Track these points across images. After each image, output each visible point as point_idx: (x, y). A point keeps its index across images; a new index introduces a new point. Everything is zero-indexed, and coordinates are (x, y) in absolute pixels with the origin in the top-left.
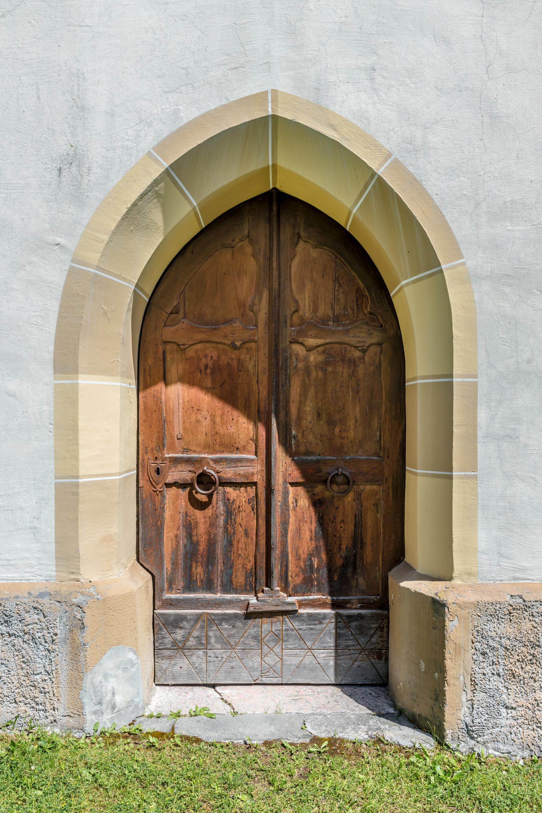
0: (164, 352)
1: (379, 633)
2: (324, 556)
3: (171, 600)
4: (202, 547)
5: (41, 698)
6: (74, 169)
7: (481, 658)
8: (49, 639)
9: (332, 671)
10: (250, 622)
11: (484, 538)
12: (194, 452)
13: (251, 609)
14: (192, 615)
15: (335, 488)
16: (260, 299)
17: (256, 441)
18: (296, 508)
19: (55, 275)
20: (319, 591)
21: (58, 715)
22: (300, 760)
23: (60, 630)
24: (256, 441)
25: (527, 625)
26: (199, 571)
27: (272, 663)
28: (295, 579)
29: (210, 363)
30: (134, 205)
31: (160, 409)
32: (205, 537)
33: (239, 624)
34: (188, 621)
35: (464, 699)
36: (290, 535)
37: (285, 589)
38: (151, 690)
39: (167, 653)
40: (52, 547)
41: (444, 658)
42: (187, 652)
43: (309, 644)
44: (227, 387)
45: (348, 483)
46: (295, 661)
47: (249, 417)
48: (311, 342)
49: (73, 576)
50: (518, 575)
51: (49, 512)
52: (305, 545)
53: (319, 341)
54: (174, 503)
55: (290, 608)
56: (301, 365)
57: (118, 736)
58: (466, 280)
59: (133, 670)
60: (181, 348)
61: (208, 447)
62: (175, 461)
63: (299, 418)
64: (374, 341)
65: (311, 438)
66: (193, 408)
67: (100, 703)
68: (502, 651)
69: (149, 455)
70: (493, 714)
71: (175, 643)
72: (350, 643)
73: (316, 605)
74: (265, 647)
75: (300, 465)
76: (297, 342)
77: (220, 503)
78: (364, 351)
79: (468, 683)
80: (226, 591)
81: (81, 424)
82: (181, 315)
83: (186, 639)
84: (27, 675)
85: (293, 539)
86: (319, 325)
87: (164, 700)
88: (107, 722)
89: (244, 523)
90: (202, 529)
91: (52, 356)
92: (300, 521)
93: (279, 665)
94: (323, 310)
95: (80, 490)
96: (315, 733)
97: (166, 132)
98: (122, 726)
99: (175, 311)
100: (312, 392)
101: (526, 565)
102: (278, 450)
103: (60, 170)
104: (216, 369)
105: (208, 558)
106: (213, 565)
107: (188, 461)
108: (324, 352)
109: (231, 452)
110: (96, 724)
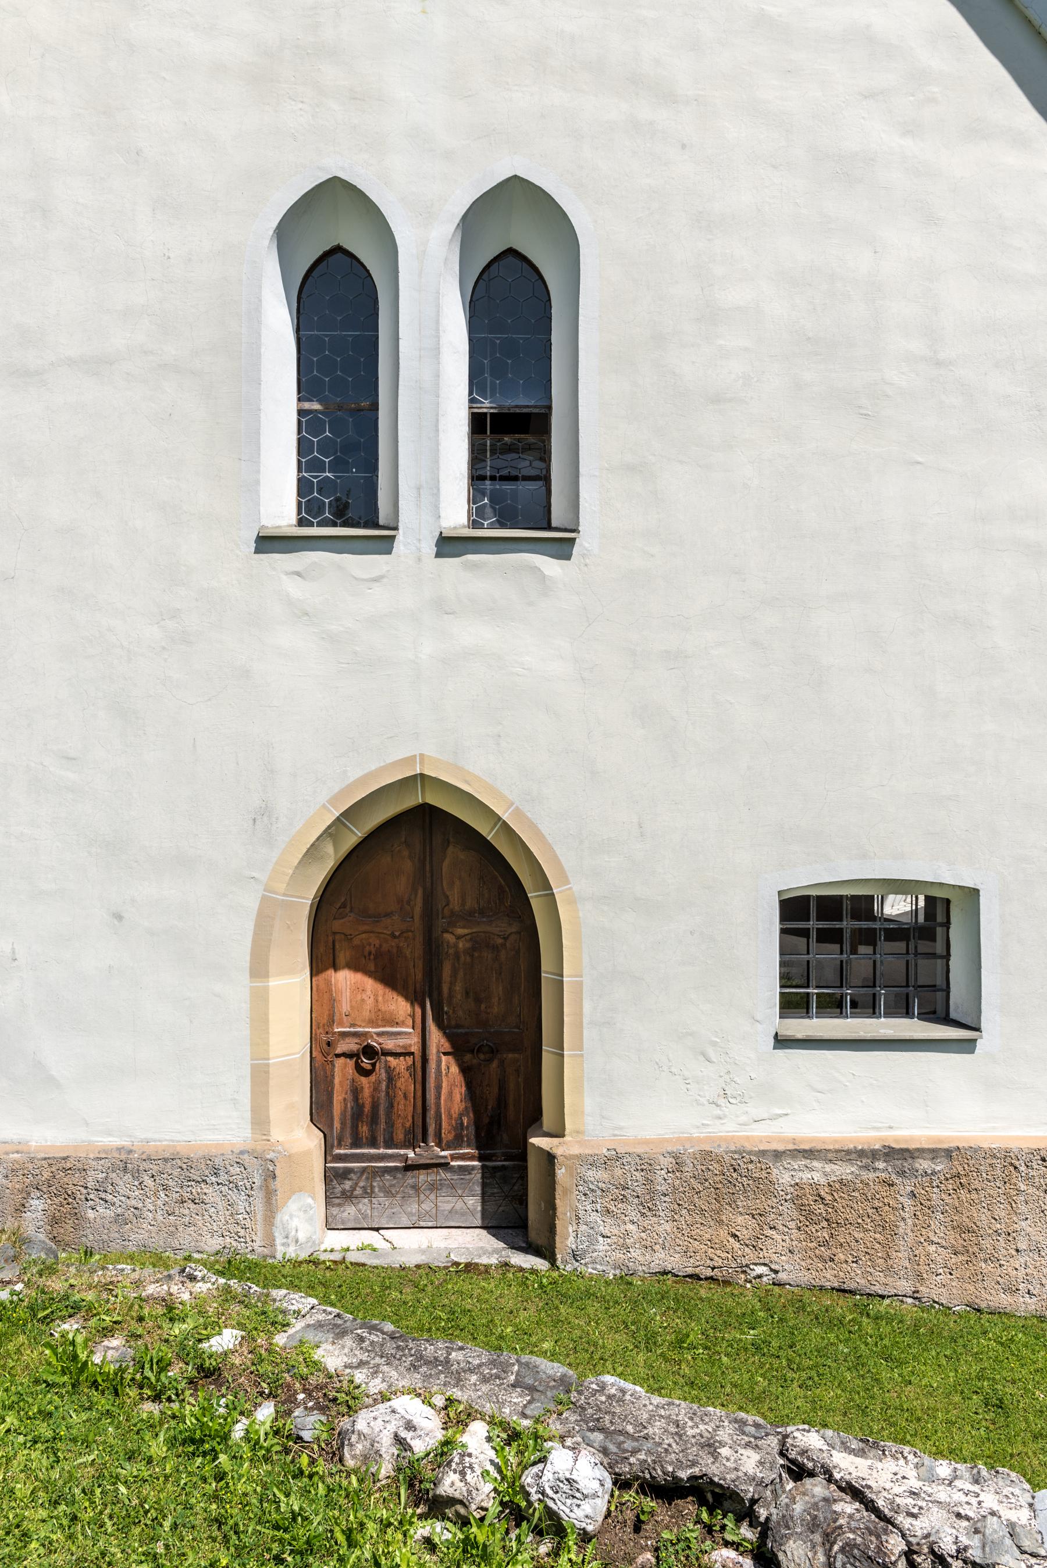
0: (334, 942)
1: (520, 1182)
2: (471, 1115)
3: (340, 1155)
4: (367, 1109)
5: (242, 1233)
6: (265, 818)
7: (583, 1198)
8: (249, 1187)
9: (479, 1215)
10: (409, 1173)
11: (589, 1103)
12: (360, 1026)
13: (410, 1162)
14: (358, 1167)
15: (482, 1056)
16: (416, 895)
17: (413, 1016)
18: (448, 1076)
19: (251, 901)
20: (469, 1146)
21: (256, 1245)
22: (440, 1276)
23: (258, 1180)
24: (413, 1016)
25: (618, 1172)
26: (364, 1130)
27: (428, 1209)
28: (447, 1135)
29: (373, 951)
30: (312, 845)
31: (331, 991)
32: (369, 1100)
33: (399, 1176)
34: (355, 1173)
35: (571, 1231)
36: (443, 1098)
37: (439, 1144)
38: (324, 1232)
39: (337, 1201)
40: (248, 1115)
41: (555, 1199)
42: (355, 1201)
43: (460, 1192)
44: (389, 975)
45: (492, 1052)
46: (448, 1207)
48: (460, 931)
49: (265, 1137)
50: (616, 1132)
51: (246, 1086)
52: (456, 1107)
53: (466, 931)
54: (343, 1071)
55: (443, 1161)
56: (451, 951)
57: (301, 1262)
58: (572, 901)
59: (311, 1212)
60: (348, 938)
61: (372, 1023)
63: (451, 996)
64: (514, 930)
65: (460, 1013)
66: (359, 989)
67: (287, 1237)
68: (599, 1193)
69: (321, 1030)
70: (592, 1242)
71: (343, 1192)
72: (495, 1190)
73: (466, 1159)
74: (422, 1195)
75: (449, 1037)
76: (447, 932)
77: (383, 1071)
78: (506, 939)
79: (574, 1218)
80: (388, 1147)
81: (271, 1017)
82: (348, 909)
83: (353, 1189)
84: (232, 1215)
85: (445, 1101)
86: (467, 917)
87: (337, 1241)
88: (292, 1252)
89: (403, 1088)
90: (367, 1092)
91: (248, 965)
92: (452, 1086)
93: (434, 1211)
94: (470, 903)
95: (271, 1069)
96: (456, 1259)
97: (337, 789)
98: (303, 1255)
99: (344, 906)
100: (461, 974)
101: (622, 1124)
103: (254, 820)
104: (379, 955)
105: (372, 1118)
106: (377, 1124)
107: (355, 1034)
108: (471, 939)
109: (392, 1026)
110: (285, 1254)
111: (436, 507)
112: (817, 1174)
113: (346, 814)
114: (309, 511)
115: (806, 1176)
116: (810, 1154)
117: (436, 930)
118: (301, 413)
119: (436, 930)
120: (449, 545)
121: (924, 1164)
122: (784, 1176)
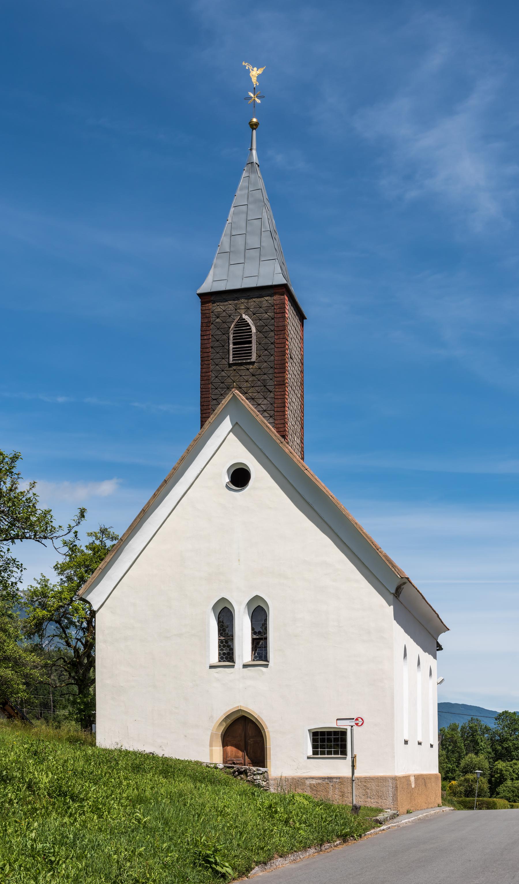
19: (209, 733)
44: (237, 747)
47: (241, 751)
61: (235, 758)
62: (229, 760)
66: (232, 751)
102: (246, 757)
111: (242, 659)
112: (314, 782)
113: (226, 717)
114: (221, 659)
115: (312, 782)
116: (313, 778)
117: (244, 735)
118: (219, 640)
119: (244, 735)
120: (245, 666)
121: (335, 780)
122: (308, 782)
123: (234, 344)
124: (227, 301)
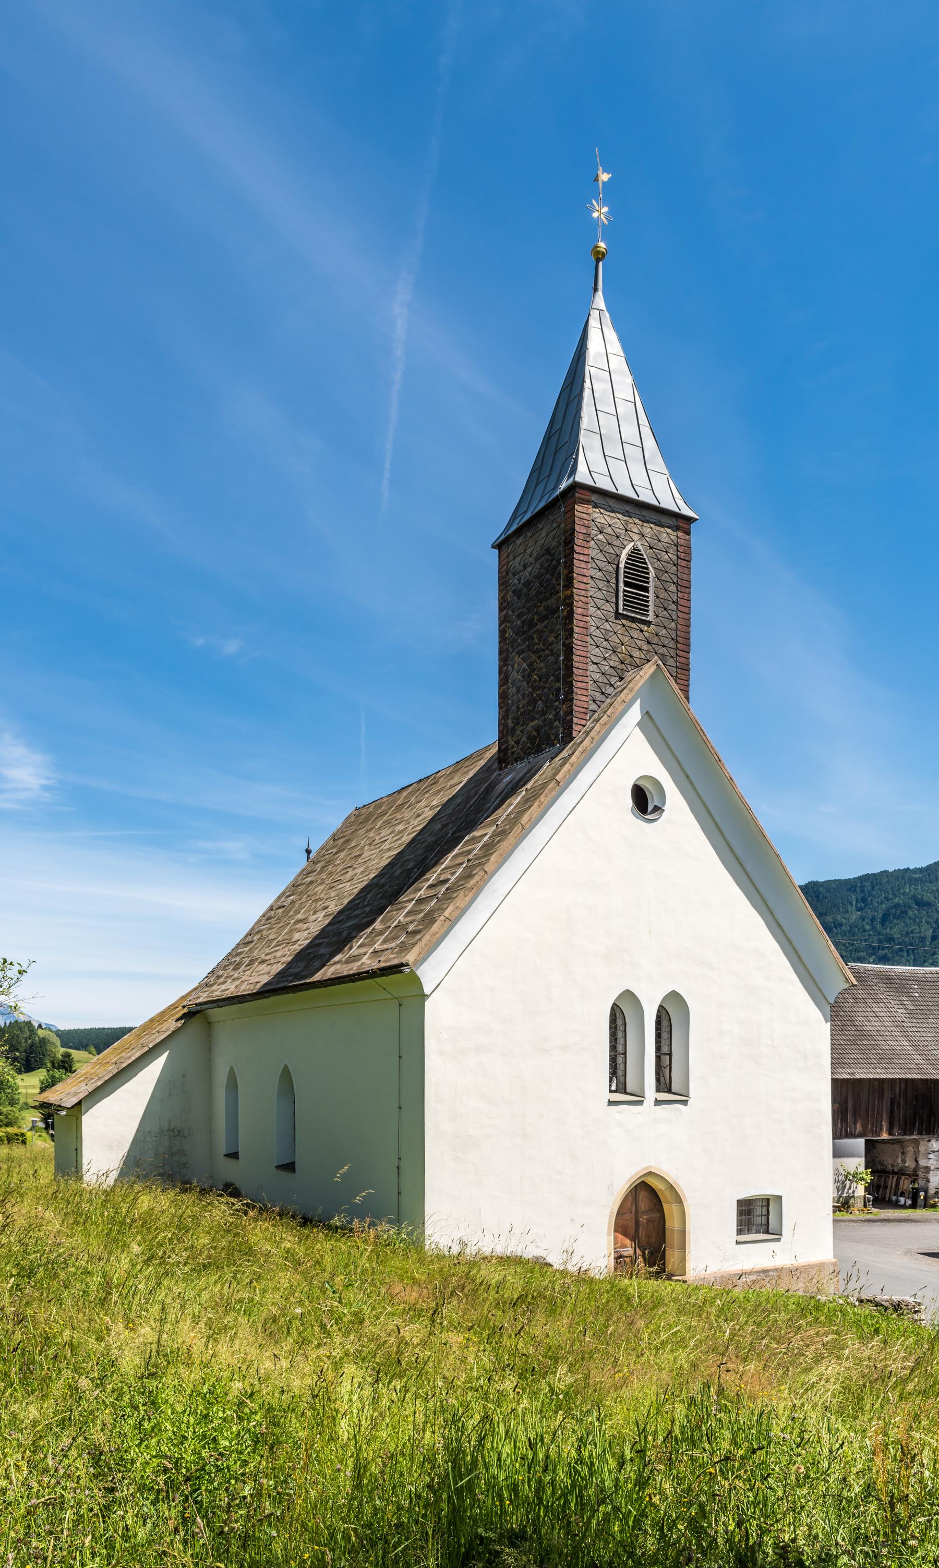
86: (645, 1213)
117: (648, 1220)
119: (648, 1220)
123: (626, 584)
124: (614, 512)
